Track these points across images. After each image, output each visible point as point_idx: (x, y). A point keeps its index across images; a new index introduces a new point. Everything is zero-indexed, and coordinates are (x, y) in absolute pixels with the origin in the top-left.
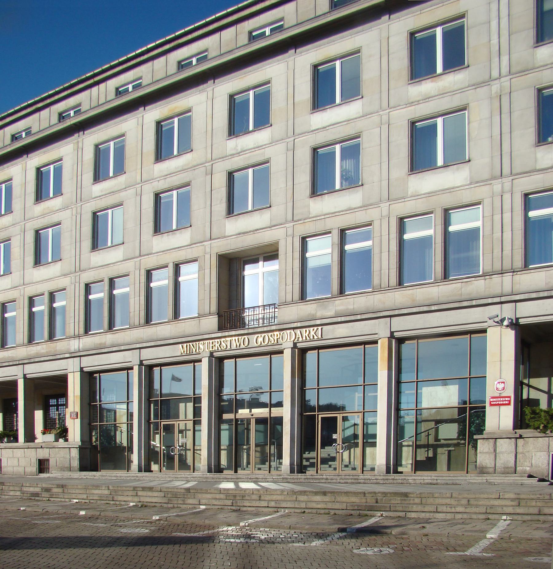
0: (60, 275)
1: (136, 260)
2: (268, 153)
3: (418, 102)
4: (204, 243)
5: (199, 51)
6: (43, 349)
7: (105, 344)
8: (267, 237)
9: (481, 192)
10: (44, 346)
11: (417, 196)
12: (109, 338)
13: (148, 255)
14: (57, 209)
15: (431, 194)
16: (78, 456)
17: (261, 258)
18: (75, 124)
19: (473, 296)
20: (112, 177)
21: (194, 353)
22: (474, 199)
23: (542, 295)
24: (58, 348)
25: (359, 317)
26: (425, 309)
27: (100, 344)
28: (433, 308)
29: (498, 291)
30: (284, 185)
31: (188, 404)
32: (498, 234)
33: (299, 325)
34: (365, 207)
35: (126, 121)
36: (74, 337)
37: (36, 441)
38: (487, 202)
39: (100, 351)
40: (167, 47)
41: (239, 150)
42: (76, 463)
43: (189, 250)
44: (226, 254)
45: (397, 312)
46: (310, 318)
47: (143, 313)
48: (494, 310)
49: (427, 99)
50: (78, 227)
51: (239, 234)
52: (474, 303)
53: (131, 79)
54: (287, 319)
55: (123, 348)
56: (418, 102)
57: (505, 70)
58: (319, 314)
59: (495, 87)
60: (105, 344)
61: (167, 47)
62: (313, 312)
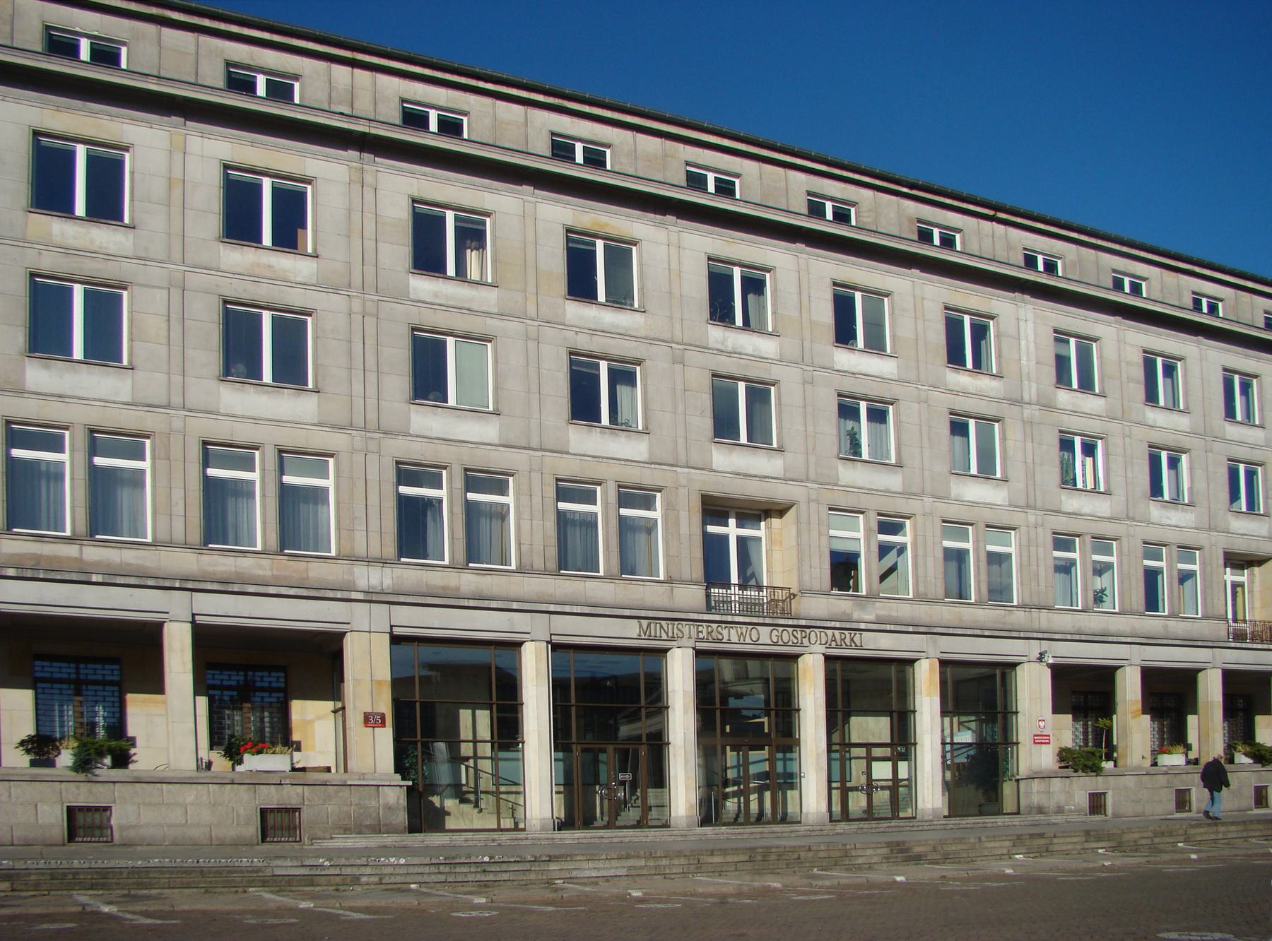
0: (315, 421)
1: (531, 452)
2: (775, 372)
3: (957, 393)
4: (678, 469)
5: (450, 105)
6: (261, 567)
7: (458, 589)
8: (780, 492)
9: (335, 441)
10: (266, 562)
11: (960, 502)
12: (467, 581)
13: (561, 453)
14: (299, 279)
15: (974, 504)
16: (403, 802)
17: (732, 513)
18: (364, 135)
19: (1016, 627)
20: (739, 328)
21: (664, 636)
22: (1005, 522)
23: (1069, 637)
24: (311, 574)
25: (911, 629)
26: (979, 632)
27: (444, 588)
28: (987, 633)
29: (1036, 627)
30: (801, 428)
31: (478, 712)
32: (1034, 567)
33: (838, 625)
34: (906, 494)
35: (495, 191)
36: (369, 561)
37: (131, 766)
38: (1023, 529)
39: (451, 601)
40: (540, 98)
41: (730, 349)
42: (402, 818)
43: (647, 472)
44: (712, 496)
45: (951, 631)
46: (844, 618)
47: (553, 552)
48: (1034, 648)
49: (966, 394)
50: (370, 342)
51: (738, 474)
52: (1022, 635)
53: (442, 103)
54: (813, 613)
55: (515, 606)
56: (957, 393)
57: (1034, 398)
58: (856, 616)
59: (1028, 412)
60: (458, 589)
61: (540, 98)
62: (848, 611)
